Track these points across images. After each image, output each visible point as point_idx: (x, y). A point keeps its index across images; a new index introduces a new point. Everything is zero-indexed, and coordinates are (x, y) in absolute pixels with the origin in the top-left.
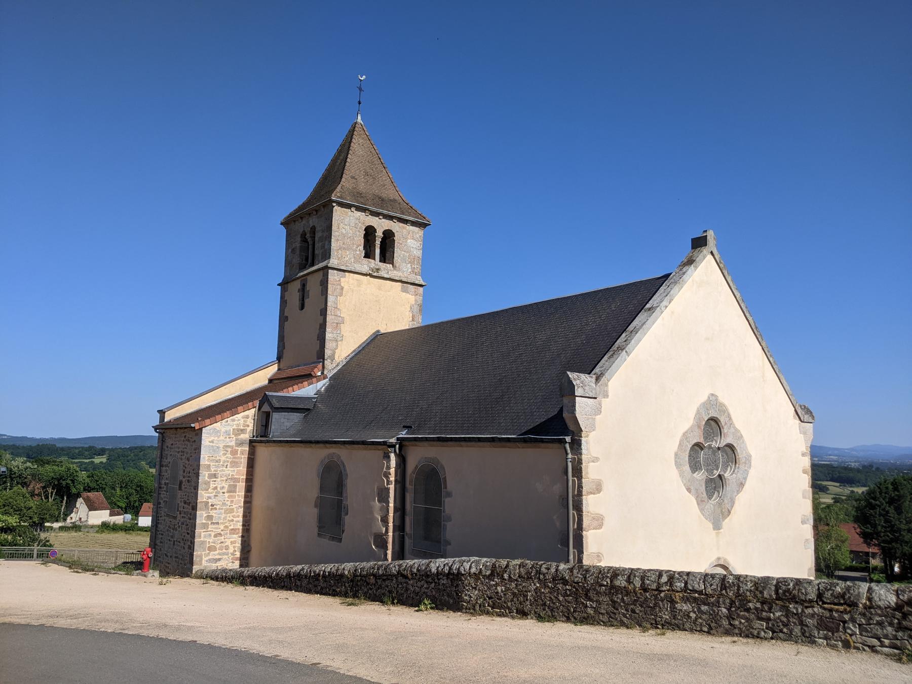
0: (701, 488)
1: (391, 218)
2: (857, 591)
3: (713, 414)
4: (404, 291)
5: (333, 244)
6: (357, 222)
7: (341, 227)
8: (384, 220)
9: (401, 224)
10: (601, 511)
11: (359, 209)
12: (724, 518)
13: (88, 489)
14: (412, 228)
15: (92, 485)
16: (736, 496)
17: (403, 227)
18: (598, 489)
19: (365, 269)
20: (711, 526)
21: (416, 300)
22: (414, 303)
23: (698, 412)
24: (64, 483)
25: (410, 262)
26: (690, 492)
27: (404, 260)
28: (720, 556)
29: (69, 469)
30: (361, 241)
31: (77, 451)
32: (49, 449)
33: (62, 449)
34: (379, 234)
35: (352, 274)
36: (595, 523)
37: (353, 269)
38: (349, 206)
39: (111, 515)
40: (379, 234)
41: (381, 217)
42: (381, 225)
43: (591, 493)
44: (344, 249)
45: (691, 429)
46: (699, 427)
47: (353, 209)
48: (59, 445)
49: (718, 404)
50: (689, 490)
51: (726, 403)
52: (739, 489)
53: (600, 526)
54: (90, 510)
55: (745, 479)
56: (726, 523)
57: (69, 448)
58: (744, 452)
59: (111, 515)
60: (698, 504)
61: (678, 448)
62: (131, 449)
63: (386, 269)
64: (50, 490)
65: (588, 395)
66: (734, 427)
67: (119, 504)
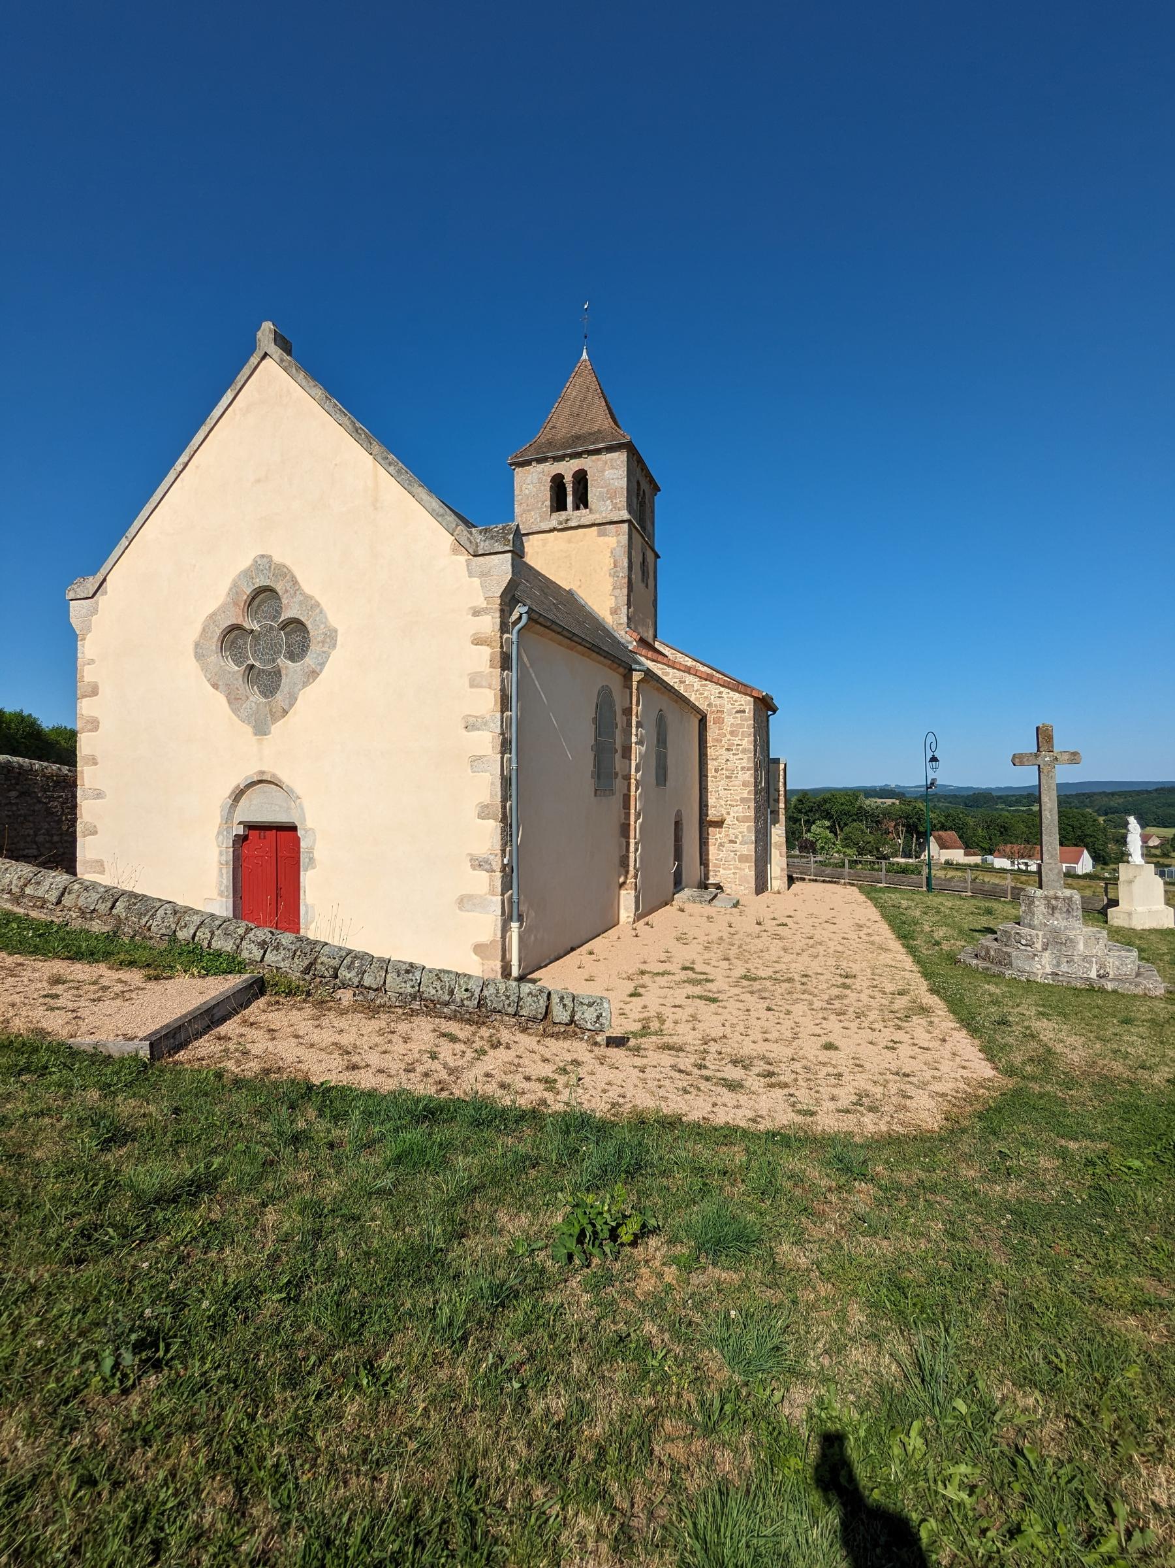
0: (235, 682)
1: (578, 455)
2: (1137, 942)
3: (261, 582)
4: (600, 535)
5: (516, 511)
6: (541, 476)
7: (523, 488)
8: (572, 461)
9: (594, 457)
10: (95, 714)
11: (540, 461)
12: (275, 720)
13: (943, 828)
14: (609, 456)
15: (948, 824)
16: (300, 690)
17: (598, 460)
18: (94, 691)
19: (553, 523)
20: (248, 730)
21: (618, 542)
22: (615, 545)
23: (235, 584)
24: (911, 821)
25: (609, 498)
26: (217, 689)
27: (601, 498)
28: (264, 769)
29: (914, 808)
30: (547, 494)
31: (1014, 799)
32: (985, 797)
33: (1000, 797)
34: (568, 479)
35: (536, 536)
36: (89, 726)
37: (535, 529)
38: (527, 463)
39: (966, 855)
40: (568, 479)
41: (568, 459)
42: (568, 469)
43: (86, 696)
44: (529, 511)
45: (223, 609)
46: (236, 604)
47: (534, 464)
48: (994, 794)
49: (273, 567)
50: (215, 686)
51: (288, 563)
52: (308, 680)
53: (96, 728)
54: (941, 848)
55: (323, 665)
56: (276, 728)
57: (1008, 796)
58: (322, 626)
59: (966, 855)
60: (229, 703)
61: (201, 636)
62: (1077, 795)
63: (584, 516)
64: (900, 828)
65: (79, 597)
66: (303, 594)
67: (981, 844)
